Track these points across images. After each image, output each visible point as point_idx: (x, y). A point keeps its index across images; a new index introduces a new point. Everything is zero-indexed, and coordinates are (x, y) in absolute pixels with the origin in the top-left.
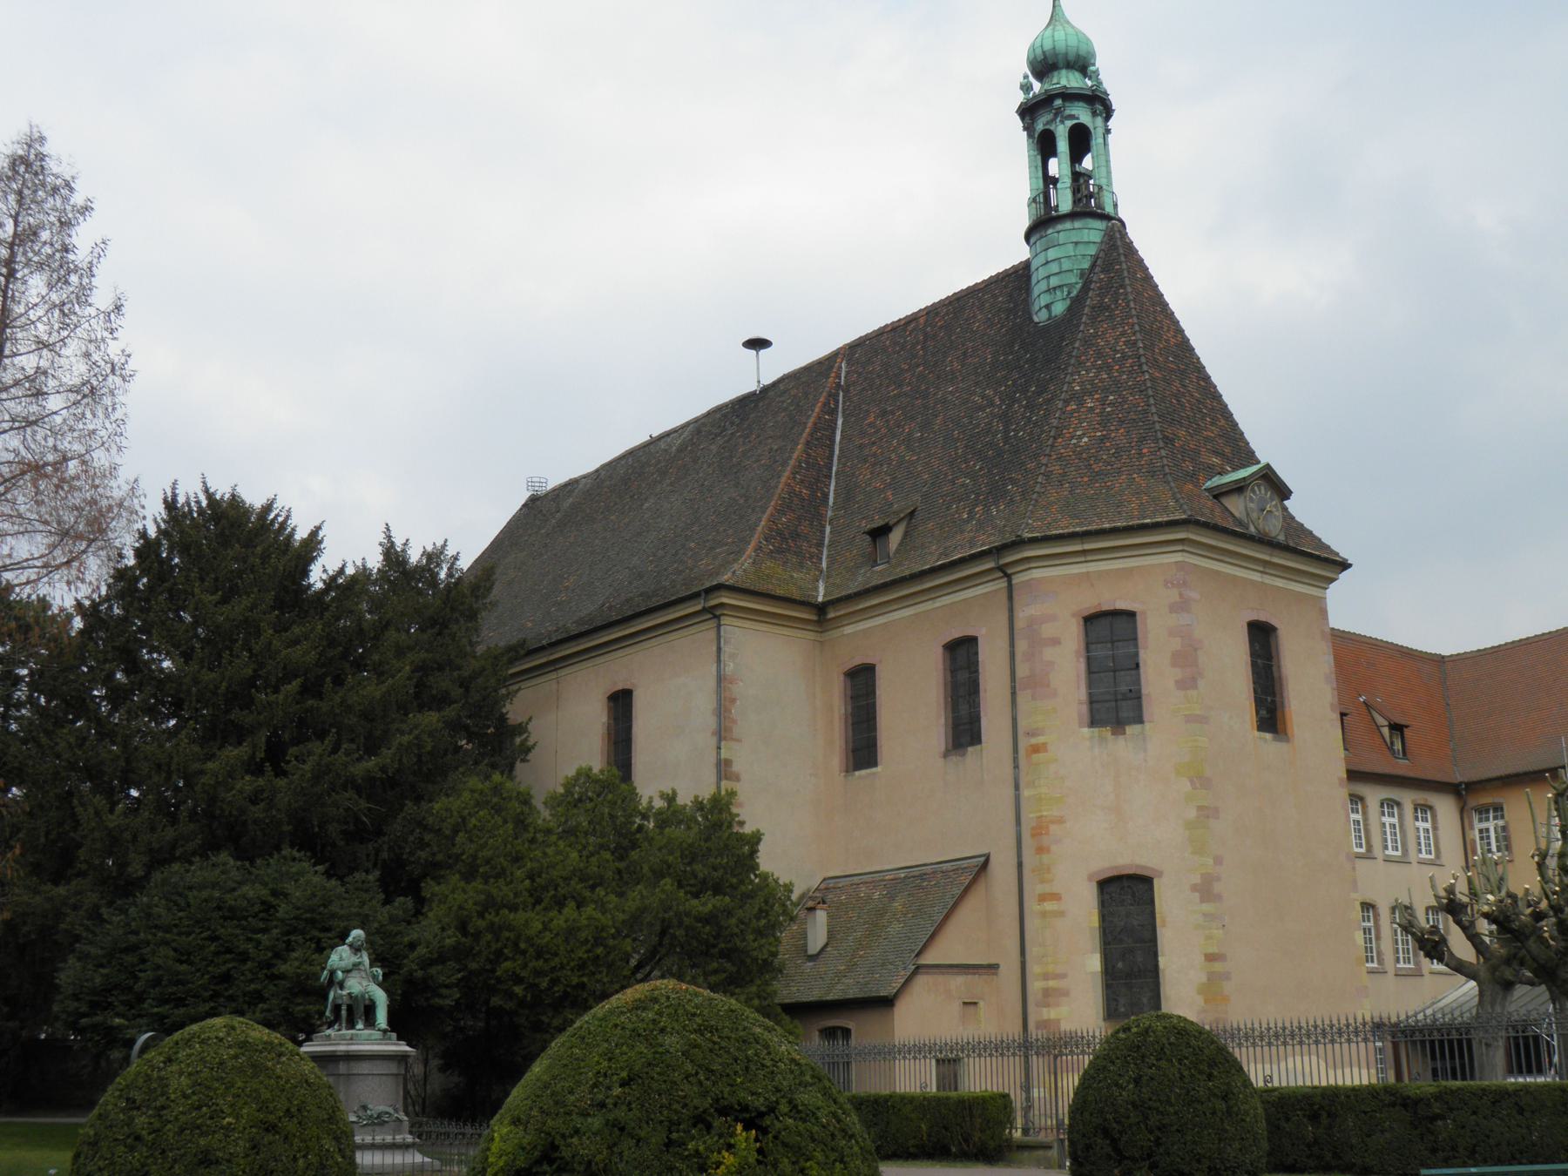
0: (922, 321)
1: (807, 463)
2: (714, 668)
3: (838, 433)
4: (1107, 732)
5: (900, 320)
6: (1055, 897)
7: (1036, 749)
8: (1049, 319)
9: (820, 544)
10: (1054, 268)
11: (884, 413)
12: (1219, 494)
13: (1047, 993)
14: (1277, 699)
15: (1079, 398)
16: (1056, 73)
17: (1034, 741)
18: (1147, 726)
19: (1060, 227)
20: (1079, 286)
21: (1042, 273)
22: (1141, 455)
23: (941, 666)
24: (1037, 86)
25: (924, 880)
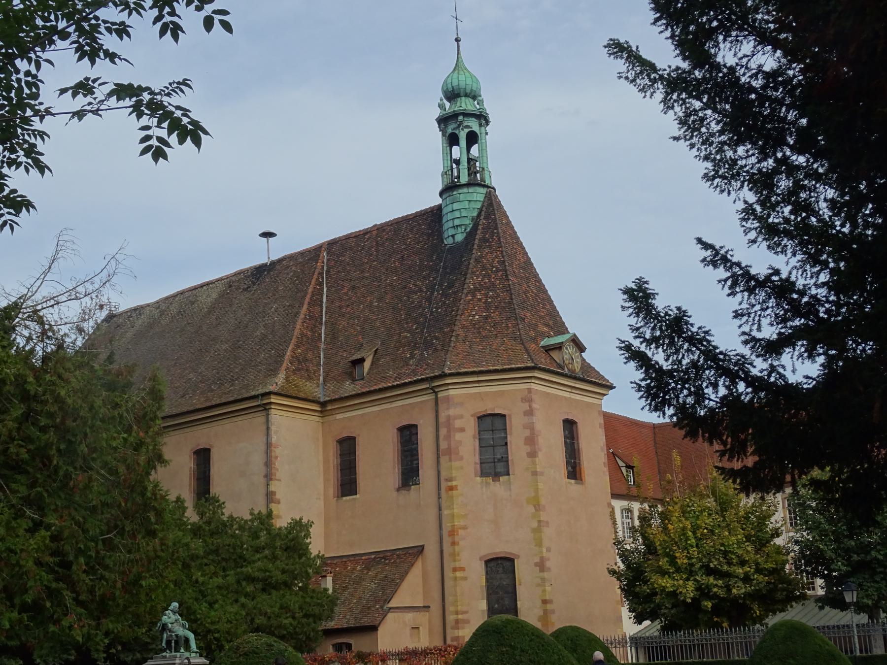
0: (374, 233)
1: (310, 316)
2: (265, 439)
3: (325, 296)
4: (490, 480)
5: (360, 231)
6: (462, 569)
7: (451, 488)
8: (454, 243)
9: (319, 364)
10: (457, 214)
11: (354, 288)
12: (548, 349)
13: (457, 621)
14: (577, 461)
15: (473, 292)
16: (459, 99)
17: (450, 484)
18: (511, 476)
19: (460, 191)
20: (471, 226)
21: (450, 216)
22: (507, 327)
23: (396, 440)
24: (447, 105)
25: (386, 559)
